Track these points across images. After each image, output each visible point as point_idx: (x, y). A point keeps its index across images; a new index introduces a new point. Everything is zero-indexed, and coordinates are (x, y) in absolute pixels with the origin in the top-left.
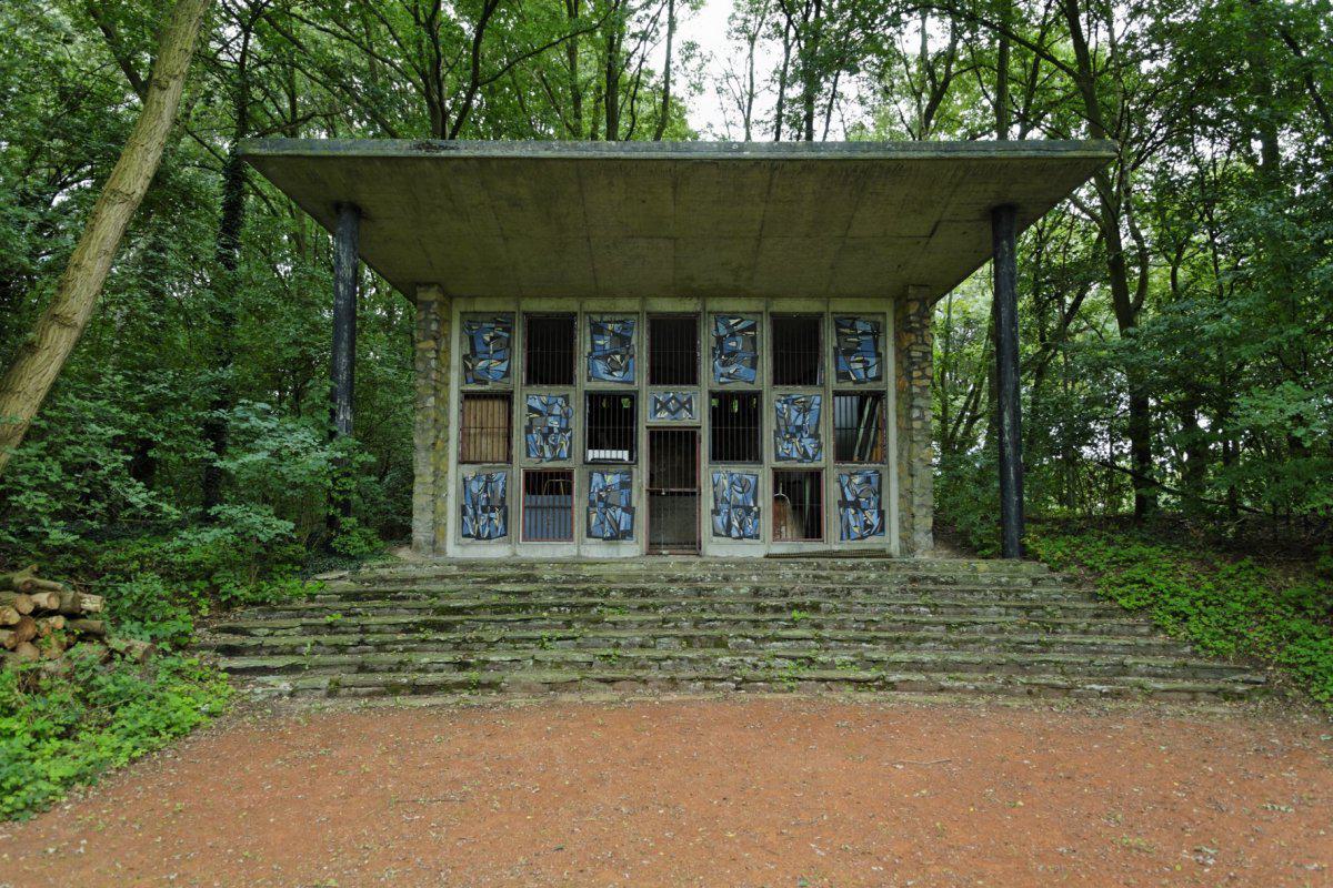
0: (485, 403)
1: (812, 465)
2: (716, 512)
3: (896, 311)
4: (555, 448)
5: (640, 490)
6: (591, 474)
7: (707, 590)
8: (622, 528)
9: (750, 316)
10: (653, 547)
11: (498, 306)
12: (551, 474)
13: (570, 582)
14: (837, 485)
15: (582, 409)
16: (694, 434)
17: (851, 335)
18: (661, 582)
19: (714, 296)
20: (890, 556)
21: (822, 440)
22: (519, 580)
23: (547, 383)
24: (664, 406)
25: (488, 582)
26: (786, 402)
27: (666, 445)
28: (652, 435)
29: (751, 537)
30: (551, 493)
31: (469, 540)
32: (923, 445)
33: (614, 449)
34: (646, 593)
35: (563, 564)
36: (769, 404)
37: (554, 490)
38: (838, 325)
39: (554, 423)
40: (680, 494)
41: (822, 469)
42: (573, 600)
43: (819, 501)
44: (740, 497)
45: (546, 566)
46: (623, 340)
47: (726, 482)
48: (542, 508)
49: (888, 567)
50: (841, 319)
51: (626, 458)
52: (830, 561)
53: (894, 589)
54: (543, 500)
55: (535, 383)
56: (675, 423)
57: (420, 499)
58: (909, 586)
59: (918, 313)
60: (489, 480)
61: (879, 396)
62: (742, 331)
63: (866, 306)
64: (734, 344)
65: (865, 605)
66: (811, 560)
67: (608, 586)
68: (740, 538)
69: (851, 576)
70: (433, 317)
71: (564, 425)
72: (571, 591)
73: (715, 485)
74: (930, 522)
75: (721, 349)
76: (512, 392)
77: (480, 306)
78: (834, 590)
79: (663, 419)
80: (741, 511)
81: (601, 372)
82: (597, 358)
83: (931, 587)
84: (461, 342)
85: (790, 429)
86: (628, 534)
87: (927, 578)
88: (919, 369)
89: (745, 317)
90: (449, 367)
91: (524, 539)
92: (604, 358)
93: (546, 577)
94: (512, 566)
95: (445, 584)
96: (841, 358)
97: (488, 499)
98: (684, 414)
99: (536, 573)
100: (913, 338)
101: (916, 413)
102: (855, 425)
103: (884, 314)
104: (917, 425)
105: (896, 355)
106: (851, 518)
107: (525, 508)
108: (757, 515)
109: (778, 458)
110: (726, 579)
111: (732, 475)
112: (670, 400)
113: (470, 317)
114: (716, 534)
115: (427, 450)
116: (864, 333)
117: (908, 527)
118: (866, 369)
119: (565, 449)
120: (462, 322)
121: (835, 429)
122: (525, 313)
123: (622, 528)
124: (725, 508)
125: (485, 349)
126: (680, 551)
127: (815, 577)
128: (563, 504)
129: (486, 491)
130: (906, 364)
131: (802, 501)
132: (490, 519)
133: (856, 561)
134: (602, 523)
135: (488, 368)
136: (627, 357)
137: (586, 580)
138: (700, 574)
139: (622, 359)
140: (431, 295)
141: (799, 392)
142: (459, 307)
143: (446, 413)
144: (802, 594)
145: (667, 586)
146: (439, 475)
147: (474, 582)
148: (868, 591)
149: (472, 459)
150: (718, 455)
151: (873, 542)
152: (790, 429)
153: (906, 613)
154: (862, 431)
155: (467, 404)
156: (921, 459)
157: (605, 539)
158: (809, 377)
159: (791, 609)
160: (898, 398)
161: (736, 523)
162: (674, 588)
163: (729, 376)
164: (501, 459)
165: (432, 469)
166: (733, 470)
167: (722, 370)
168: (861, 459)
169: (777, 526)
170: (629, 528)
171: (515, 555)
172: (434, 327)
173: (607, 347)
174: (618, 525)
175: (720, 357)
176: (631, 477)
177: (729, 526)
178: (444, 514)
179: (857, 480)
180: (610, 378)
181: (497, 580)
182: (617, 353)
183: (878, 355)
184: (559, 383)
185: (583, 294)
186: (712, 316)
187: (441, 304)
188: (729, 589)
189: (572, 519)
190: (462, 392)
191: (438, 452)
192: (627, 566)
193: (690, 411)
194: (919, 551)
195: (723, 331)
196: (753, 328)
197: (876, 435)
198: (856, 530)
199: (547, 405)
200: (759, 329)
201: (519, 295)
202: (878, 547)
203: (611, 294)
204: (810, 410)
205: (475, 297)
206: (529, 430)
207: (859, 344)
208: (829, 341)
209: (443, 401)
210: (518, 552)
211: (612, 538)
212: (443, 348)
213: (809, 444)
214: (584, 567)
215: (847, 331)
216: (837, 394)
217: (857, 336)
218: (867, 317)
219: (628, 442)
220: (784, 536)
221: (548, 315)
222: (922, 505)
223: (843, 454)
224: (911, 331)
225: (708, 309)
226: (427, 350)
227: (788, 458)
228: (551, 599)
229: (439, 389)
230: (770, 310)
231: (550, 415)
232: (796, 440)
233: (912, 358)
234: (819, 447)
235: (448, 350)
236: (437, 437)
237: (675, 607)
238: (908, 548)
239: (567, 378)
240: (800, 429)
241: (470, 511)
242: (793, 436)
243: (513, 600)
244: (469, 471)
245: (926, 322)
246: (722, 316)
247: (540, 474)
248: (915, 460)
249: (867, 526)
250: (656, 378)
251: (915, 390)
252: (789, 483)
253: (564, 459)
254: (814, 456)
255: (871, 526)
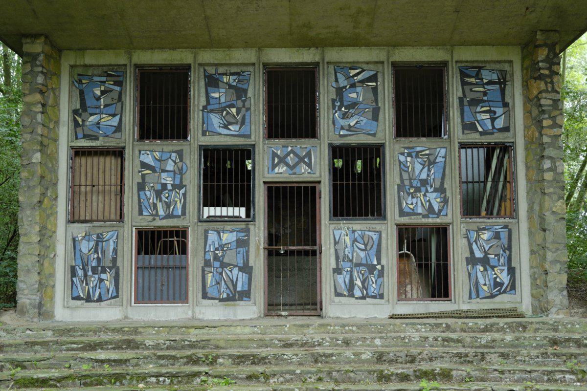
0: (96, 159)
1: (438, 221)
2: (338, 271)
3: (523, 59)
4: (168, 205)
5: (258, 248)
6: (206, 232)
7: (324, 355)
8: (239, 289)
9: (371, 66)
10: (272, 307)
11: (108, 58)
12: (165, 232)
13: (175, 348)
14: (465, 241)
15: (196, 165)
16: (314, 188)
17: (477, 84)
18: (276, 346)
19: (332, 45)
20: (521, 316)
21: (448, 194)
22: (118, 346)
23: (160, 138)
24: (283, 160)
25: (83, 349)
26: (409, 155)
27: (292, 208)
28: (270, 189)
29: (374, 297)
30: (165, 253)
31: (79, 302)
32: (555, 197)
33: (218, 205)
34: (257, 360)
35: (170, 327)
36: (391, 157)
37: (168, 249)
38: (463, 74)
39: (168, 179)
40: (299, 253)
41: (448, 225)
42: (173, 370)
43: (446, 257)
44: (362, 254)
45: (150, 330)
46: (240, 92)
47: (348, 239)
48: (155, 268)
49: (525, 328)
50: (467, 68)
51: (243, 215)
52: (460, 321)
53: (534, 353)
54: (156, 259)
55: (148, 138)
56: (294, 178)
57: (26, 258)
58: (550, 350)
59: (547, 60)
60: (100, 239)
61: (506, 149)
62: (362, 82)
63: (490, 54)
64: (354, 95)
65: (502, 372)
66: (440, 321)
67: (216, 352)
68: (363, 298)
69: (485, 338)
70: (40, 69)
71: (177, 182)
72: (174, 358)
73: (336, 243)
74: (564, 277)
75: (341, 101)
76: (124, 148)
77: (90, 58)
78: (466, 356)
79: (281, 173)
80: (364, 269)
81: (216, 125)
82: (212, 111)
83: (574, 350)
84: (70, 96)
85: (415, 183)
86: (245, 295)
87: (569, 340)
88: (550, 117)
89: (365, 66)
90: (57, 123)
91: (137, 301)
92: (220, 111)
93: (149, 343)
94: (113, 330)
95: (36, 352)
96: (467, 108)
97: (98, 258)
98: (303, 168)
99: (138, 338)
100: (542, 86)
101: (547, 164)
102: (482, 179)
103: (511, 62)
104: (548, 176)
105: (524, 104)
106: (480, 275)
107: (138, 268)
108: (381, 274)
109: (402, 213)
110: (347, 343)
111: (354, 231)
112: (288, 154)
113: (80, 71)
114: (338, 294)
115: (33, 208)
116: (491, 82)
117: (540, 283)
118: (493, 120)
119: (179, 206)
120: (71, 76)
121: (461, 183)
122: (137, 66)
123: (239, 289)
124: (347, 266)
125: (95, 103)
126: (301, 312)
127: (444, 340)
128: (178, 264)
129: (96, 251)
130: (535, 112)
131: (428, 258)
132: (101, 280)
133: (489, 321)
134: (218, 283)
135: (98, 123)
136: (244, 110)
137: (192, 346)
138: (317, 338)
139: (238, 113)
140: (37, 47)
141: (422, 144)
142: (67, 61)
143: (54, 170)
144: (431, 359)
145: (280, 351)
146: (46, 235)
147: (68, 350)
148: (503, 355)
149: (82, 218)
150: (340, 211)
151: (503, 301)
152: (415, 183)
153: (549, 380)
154: (489, 184)
155: (77, 160)
156: (554, 213)
157: (221, 300)
158: (434, 131)
159: (419, 378)
160: (527, 149)
161: (358, 283)
162: (289, 352)
163: (350, 128)
164: (113, 217)
165: (37, 228)
166: (355, 227)
167: (343, 122)
168: (490, 213)
169: (401, 285)
170: (246, 288)
171: (126, 317)
172: (40, 79)
173: (223, 100)
174: (235, 286)
175: (340, 109)
176: (248, 235)
177: (351, 286)
178: (52, 275)
179: (485, 236)
180: (225, 131)
181: (92, 347)
182: (232, 106)
183: (506, 105)
184: (172, 138)
185: (195, 46)
186: (331, 67)
187: (48, 57)
188: (349, 353)
189: (187, 280)
190: (72, 148)
191: (44, 210)
192: (239, 330)
193: (309, 165)
194: (554, 310)
195: (343, 82)
196: (374, 78)
197: (504, 187)
198: (485, 288)
199: (160, 161)
200: (380, 79)
201: (131, 47)
202: (508, 306)
203: (229, 46)
204: (434, 162)
205: (87, 49)
206: (141, 187)
207: (485, 94)
208: (454, 91)
209: (51, 159)
210: (130, 316)
211: (228, 299)
212: (50, 102)
213: (434, 199)
214: (192, 331)
215: (473, 80)
216: (463, 146)
217: (483, 85)
218: (493, 66)
219: (245, 199)
220: (409, 295)
221: (161, 67)
222: (555, 262)
223: (471, 208)
224: (540, 78)
225: (326, 60)
226: (34, 104)
227: (414, 213)
228: (151, 368)
229: (46, 146)
230: (392, 59)
231: (164, 171)
232: (421, 195)
233: (541, 106)
234: (445, 201)
235: (56, 105)
236: (43, 194)
237: (288, 376)
238: (541, 308)
239: (181, 133)
240: (424, 182)
241: (80, 272)
242: (418, 190)
243: (107, 369)
244: (79, 230)
245: (555, 68)
246: (340, 67)
247: (153, 232)
248: (547, 214)
249: (497, 284)
250: (275, 130)
251: (546, 139)
252: (414, 241)
253: (178, 217)
254: (440, 211)
255: (502, 284)
